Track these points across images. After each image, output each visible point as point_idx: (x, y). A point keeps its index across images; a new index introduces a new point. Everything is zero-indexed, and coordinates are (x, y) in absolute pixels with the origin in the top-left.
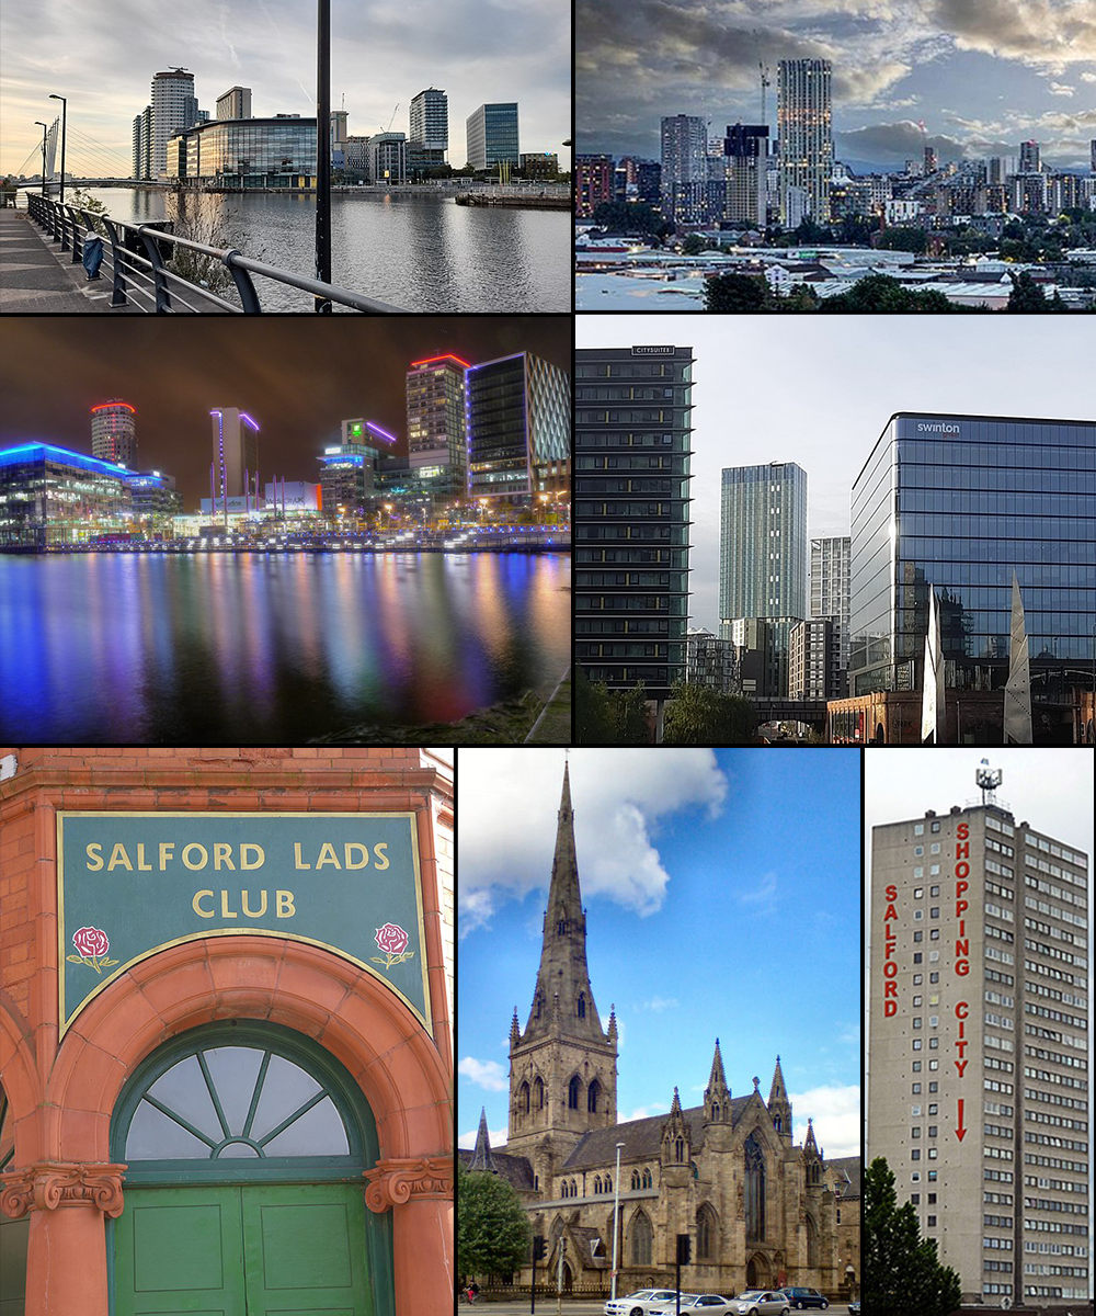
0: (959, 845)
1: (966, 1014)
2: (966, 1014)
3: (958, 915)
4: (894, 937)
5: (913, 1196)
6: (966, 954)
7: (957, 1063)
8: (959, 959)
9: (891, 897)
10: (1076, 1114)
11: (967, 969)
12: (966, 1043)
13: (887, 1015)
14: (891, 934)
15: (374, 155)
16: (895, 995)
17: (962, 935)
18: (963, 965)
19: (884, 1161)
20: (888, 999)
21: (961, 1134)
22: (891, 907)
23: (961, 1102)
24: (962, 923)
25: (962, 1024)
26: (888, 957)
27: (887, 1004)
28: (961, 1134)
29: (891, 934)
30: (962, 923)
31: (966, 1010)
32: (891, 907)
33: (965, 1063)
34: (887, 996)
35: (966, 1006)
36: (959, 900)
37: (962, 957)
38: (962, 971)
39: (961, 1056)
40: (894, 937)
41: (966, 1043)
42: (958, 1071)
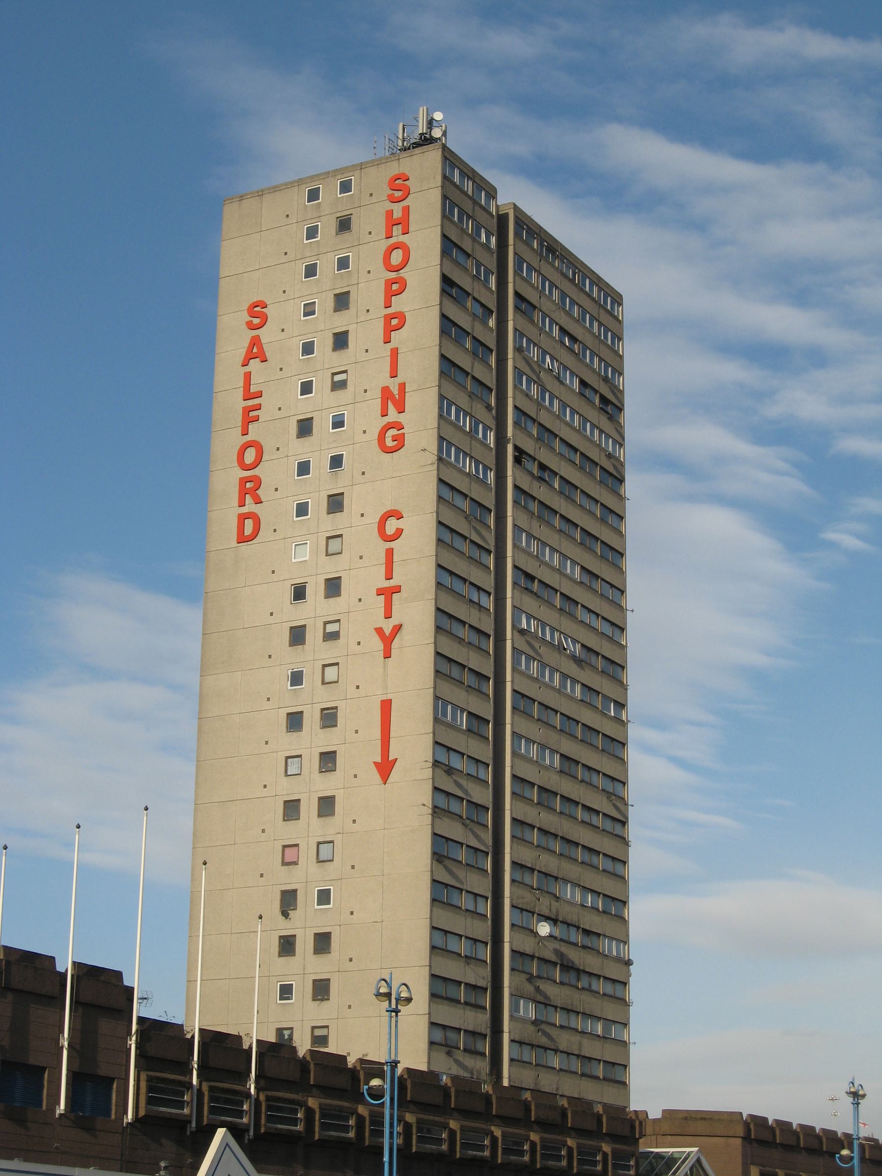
0: (390, 213)
1: (399, 533)
2: (399, 533)
3: (387, 341)
4: (259, 395)
5: (348, 1053)
6: (401, 411)
7: (379, 631)
8: (387, 420)
9: (256, 321)
10: (563, 463)
11: (400, 441)
12: (397, 589)
13: (242, 539)
14: (253, 389)
15: (472, 1123)
16: (258, 501)
17: (394, 375)
18: (392, 432)
19: (281, 954)
20: (244, 510)
21: (385, 768)
22: (256, 342)
23: (386, 706)
24: (395, 353)
25: (390, 553)
26: (245, 433)
27: (242, 518)
28: (385, 768)
29: (253, 389)
30: (395, 353)
31: (400, 524)
32: (256, 342)
33: (398, 628)
34: (242, 504)
35: (400, 517)
36: (390, 311)
37: (393, 415)
38: (389, 443)
39: (388, 615)
40: (259, 395)
41: (397, 589)
42: (380, 646)
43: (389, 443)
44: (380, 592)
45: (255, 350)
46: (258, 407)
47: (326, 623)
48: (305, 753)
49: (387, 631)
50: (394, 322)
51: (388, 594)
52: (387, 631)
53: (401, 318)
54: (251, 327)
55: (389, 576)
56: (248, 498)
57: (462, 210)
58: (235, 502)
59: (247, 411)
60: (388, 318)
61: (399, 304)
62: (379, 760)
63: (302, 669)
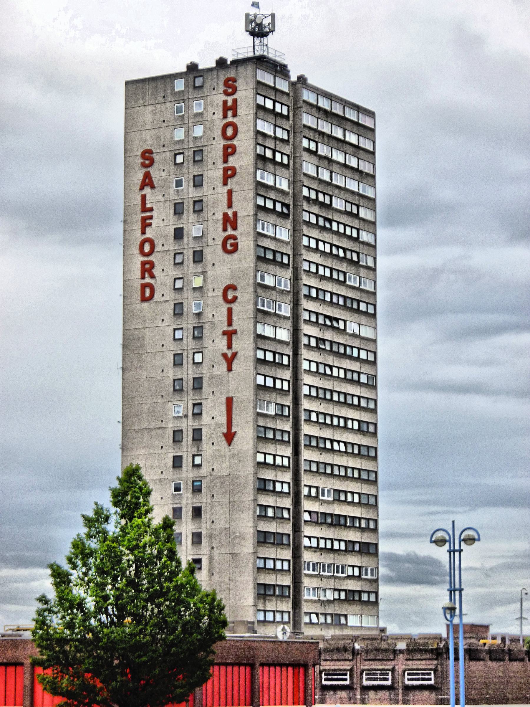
2: (235, 299)
4: (151, 210)
7: (224, 355)
8: (226, 234)
14: (148, 206)
16: (153, 276)
17: (230, 206)
18: (231, 241)
21: (229, 437)
22: (147, 175)
26: (143, 232)
27: (144, 287)
29: (148, 206)
30: (230, 193)
32: (147, 175)
37: (230, 232)
38: (229, 248)
40: (151, 210)
41: (235, 332)
42: (225, 366)
43: (229, 248)
44: (224, 333)
45: (147, 181)
46: (151, 217)
47: (193, 481)
48: (185, 327)
49: (229, 355)
50: (230, 150)
51: (230, 335)
52: (229, 355)
53: (234, 170)
54: (144, 165)
55: (230, 324)
56: (147, 275)
57: (245, 692)
58: (139, 232)
59: (144, 219)
60: (226, 170)
61: (232, 161)
62: (225, 431)
63: (182, 226)
